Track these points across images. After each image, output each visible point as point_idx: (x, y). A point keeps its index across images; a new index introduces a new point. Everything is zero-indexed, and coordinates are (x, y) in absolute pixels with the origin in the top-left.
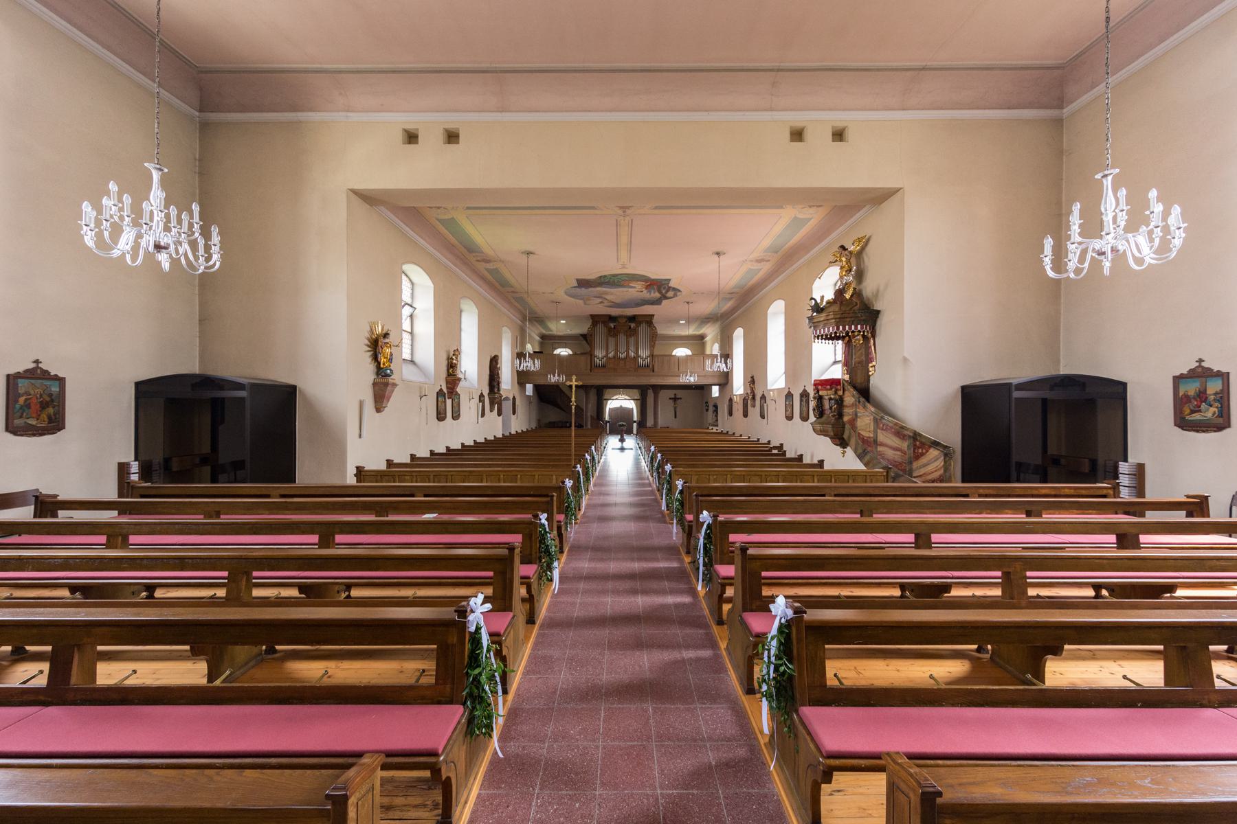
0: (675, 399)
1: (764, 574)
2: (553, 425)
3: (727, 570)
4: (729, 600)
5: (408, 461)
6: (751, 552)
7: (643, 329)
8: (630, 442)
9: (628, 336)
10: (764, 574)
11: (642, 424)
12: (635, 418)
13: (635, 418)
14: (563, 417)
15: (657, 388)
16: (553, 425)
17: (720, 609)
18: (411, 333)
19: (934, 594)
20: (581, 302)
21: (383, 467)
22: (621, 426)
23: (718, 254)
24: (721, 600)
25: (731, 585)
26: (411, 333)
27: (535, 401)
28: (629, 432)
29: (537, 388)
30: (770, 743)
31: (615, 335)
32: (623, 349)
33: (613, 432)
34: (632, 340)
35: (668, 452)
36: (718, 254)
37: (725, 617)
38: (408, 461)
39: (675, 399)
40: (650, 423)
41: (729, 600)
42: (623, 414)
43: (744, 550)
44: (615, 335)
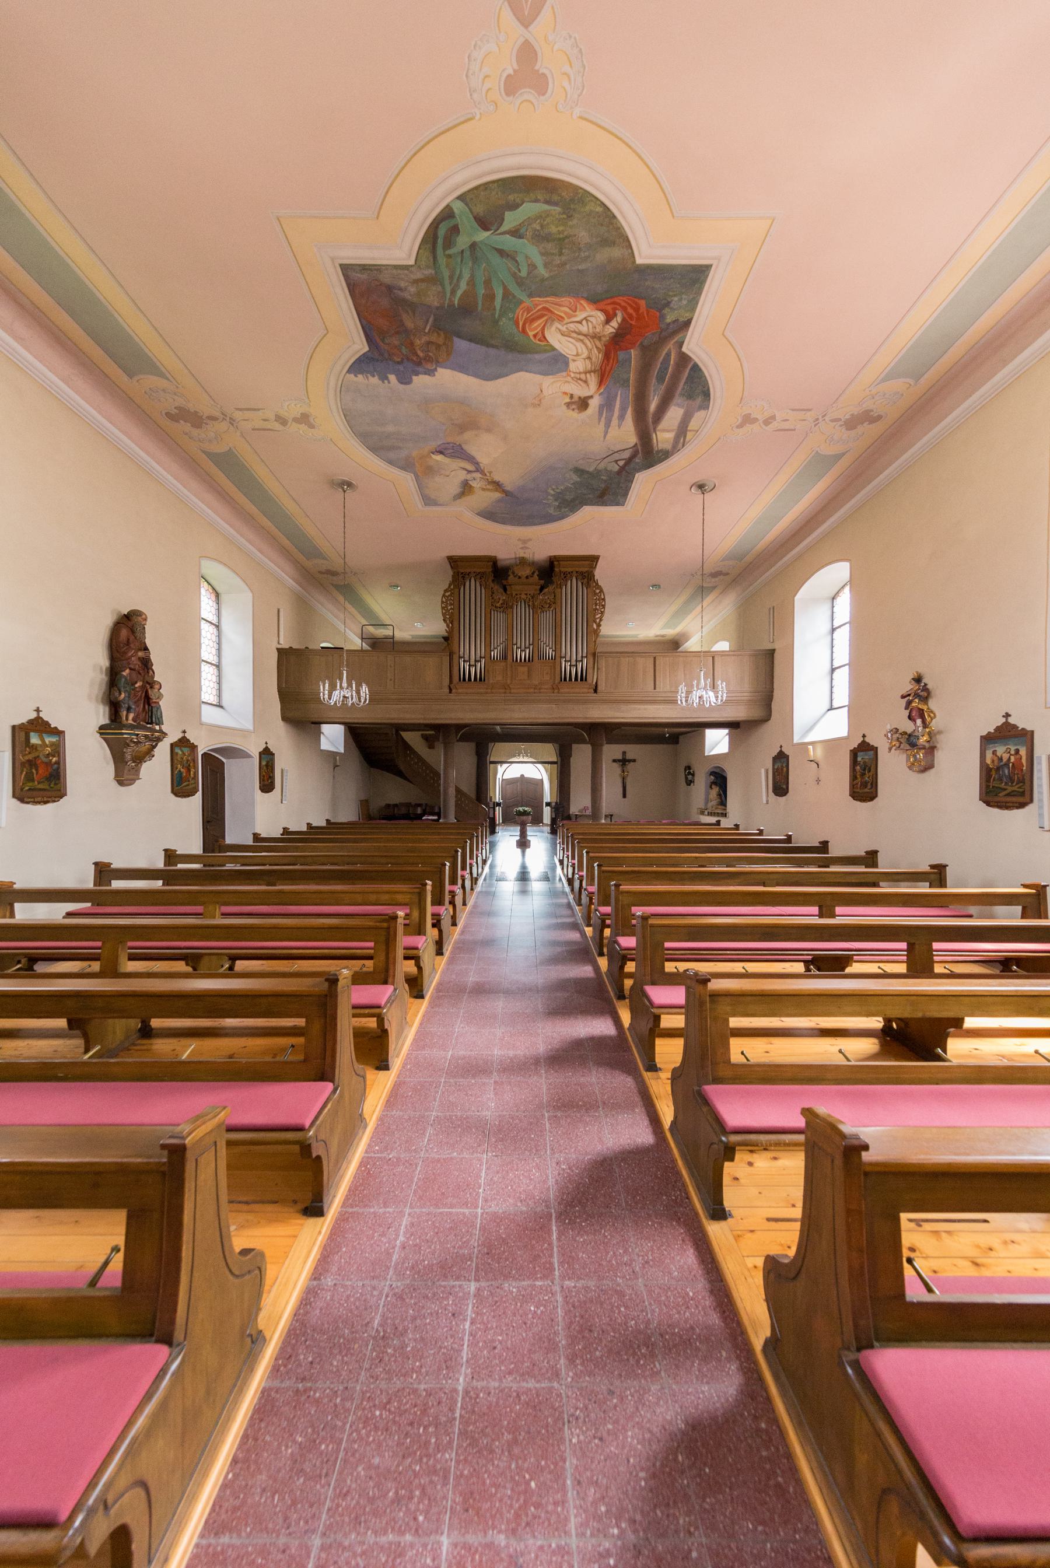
0: (624, 762)
1: (667, 945)
2: (392, 814)
3: (628, 942)
4: (630, 975)
5: (305, 829)
6: (651, 921)
7: (571, 590)
8: (539, 841)
9: (537, 608)
10: (667, 945)
11: (561, 812)
12: (547, 797)
13: (547, 797)
14: (414, 792)
15: (599, 733)
16: (392, 814)
17: (602, 932)
18: (218, 666)
19: (834, 965)
20: (406, 480)
21: (324, 824)
22: (522, 810)
23: (701, 487)
24: (621, 974)
25: (632, 960)
26: (218, 666)
27: (354, 765)
28: (537, 820)
29: (356, 733)
30: (671, 1129)
31: (506, 607)
32: (521, 632)
33: (509, 819)
34: (546, 618)
35: (610, 866)
36: (701, 487)
37: (627, 992)
38: (305, 829)
39: (624, 762)
40: (580, 801)
41: (608, 926)
42: (527, 790)
43: (645, 918)
44: (506, 607)
